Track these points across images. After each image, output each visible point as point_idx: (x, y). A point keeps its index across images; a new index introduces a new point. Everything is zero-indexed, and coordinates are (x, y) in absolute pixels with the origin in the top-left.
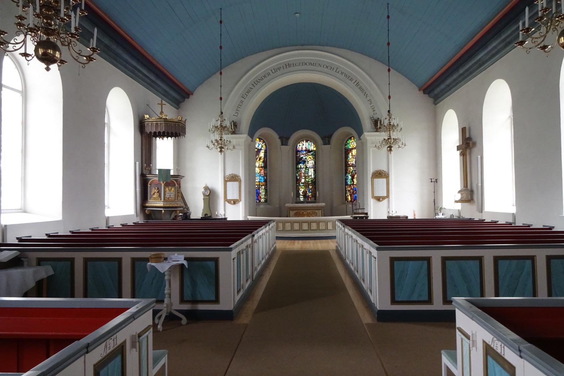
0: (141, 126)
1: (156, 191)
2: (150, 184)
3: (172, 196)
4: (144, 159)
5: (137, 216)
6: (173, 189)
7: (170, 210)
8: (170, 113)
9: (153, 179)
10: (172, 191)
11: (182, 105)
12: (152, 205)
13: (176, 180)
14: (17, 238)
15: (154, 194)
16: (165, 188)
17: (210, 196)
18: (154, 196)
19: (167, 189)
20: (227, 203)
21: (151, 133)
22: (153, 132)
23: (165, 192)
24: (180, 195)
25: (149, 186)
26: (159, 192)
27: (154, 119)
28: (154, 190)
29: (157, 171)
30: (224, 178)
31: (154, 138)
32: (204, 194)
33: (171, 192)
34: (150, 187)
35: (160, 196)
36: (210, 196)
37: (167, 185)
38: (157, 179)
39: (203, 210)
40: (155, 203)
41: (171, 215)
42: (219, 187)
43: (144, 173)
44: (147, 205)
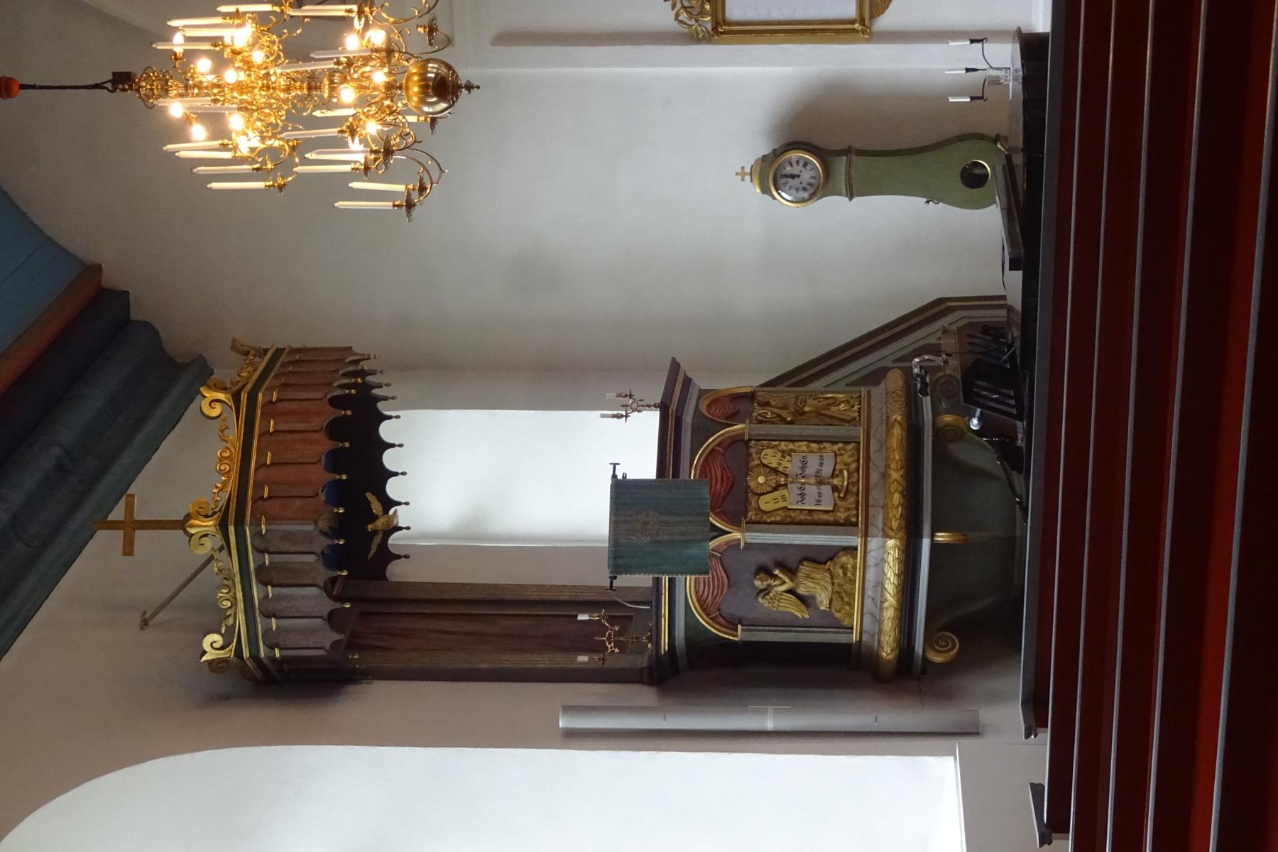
0: (292, 684)
1: (782, 584)
2: (732, 624)
3: (821, 461)
4: (543, 661)
5: (971, 731)
6: (771, 457)
7: (931, 487)
8: (193, 463)
9: (685, 601)
10: (791, 466)
11: (176, 339)
12: (889, 614)
13: (703, 429)
14: (1045, 840)
15: (805, 600)
16: (762, 522)
17: (825, 148)
18: (823, 599)
19: (767, 503)
20: (886, 21)
21: (333, 619)
22: (327, 606)
23: (791, 521)
24: (814, 383)
25: (740, 635)
26: (787, 563)
27: (230, 599)
28: (778, 600)
29: (624, 581)
30: (694, 38)
31: (396, 571)
32: (817, 191)
33: (799, 474)
34: (751, 624)
35: (821, 558)
36: (825, 148)
37: (734, 504)
38: (687, 584)
39: (932, 197)
40: (876, 584)
41: (972, 474)
42: (763, 80)
43: (642, 661)
44: (887, 651)
